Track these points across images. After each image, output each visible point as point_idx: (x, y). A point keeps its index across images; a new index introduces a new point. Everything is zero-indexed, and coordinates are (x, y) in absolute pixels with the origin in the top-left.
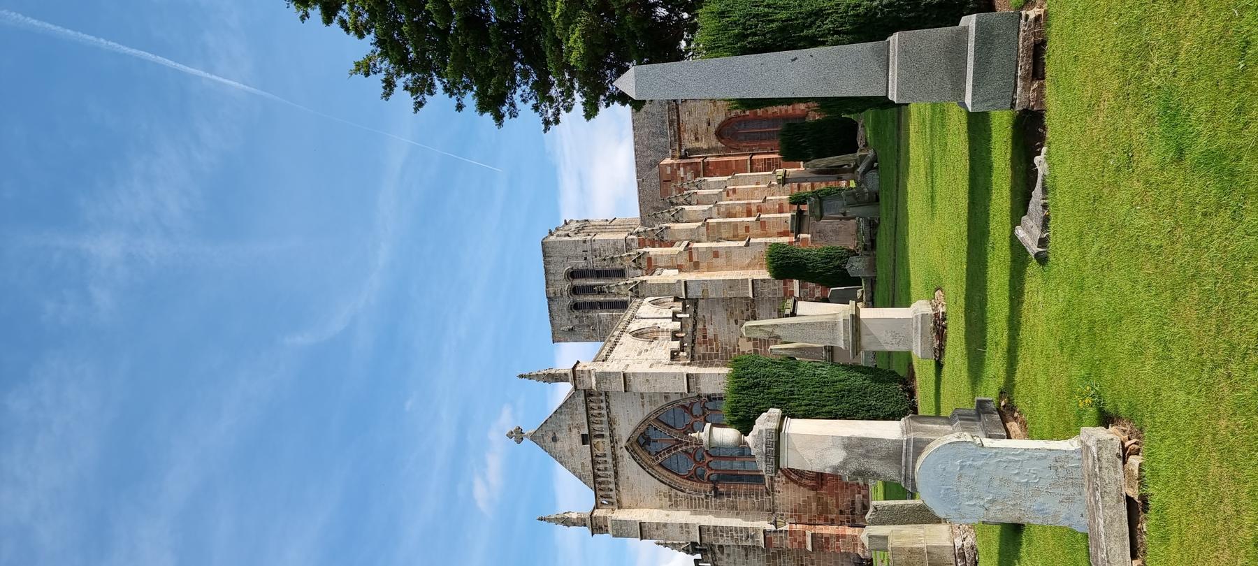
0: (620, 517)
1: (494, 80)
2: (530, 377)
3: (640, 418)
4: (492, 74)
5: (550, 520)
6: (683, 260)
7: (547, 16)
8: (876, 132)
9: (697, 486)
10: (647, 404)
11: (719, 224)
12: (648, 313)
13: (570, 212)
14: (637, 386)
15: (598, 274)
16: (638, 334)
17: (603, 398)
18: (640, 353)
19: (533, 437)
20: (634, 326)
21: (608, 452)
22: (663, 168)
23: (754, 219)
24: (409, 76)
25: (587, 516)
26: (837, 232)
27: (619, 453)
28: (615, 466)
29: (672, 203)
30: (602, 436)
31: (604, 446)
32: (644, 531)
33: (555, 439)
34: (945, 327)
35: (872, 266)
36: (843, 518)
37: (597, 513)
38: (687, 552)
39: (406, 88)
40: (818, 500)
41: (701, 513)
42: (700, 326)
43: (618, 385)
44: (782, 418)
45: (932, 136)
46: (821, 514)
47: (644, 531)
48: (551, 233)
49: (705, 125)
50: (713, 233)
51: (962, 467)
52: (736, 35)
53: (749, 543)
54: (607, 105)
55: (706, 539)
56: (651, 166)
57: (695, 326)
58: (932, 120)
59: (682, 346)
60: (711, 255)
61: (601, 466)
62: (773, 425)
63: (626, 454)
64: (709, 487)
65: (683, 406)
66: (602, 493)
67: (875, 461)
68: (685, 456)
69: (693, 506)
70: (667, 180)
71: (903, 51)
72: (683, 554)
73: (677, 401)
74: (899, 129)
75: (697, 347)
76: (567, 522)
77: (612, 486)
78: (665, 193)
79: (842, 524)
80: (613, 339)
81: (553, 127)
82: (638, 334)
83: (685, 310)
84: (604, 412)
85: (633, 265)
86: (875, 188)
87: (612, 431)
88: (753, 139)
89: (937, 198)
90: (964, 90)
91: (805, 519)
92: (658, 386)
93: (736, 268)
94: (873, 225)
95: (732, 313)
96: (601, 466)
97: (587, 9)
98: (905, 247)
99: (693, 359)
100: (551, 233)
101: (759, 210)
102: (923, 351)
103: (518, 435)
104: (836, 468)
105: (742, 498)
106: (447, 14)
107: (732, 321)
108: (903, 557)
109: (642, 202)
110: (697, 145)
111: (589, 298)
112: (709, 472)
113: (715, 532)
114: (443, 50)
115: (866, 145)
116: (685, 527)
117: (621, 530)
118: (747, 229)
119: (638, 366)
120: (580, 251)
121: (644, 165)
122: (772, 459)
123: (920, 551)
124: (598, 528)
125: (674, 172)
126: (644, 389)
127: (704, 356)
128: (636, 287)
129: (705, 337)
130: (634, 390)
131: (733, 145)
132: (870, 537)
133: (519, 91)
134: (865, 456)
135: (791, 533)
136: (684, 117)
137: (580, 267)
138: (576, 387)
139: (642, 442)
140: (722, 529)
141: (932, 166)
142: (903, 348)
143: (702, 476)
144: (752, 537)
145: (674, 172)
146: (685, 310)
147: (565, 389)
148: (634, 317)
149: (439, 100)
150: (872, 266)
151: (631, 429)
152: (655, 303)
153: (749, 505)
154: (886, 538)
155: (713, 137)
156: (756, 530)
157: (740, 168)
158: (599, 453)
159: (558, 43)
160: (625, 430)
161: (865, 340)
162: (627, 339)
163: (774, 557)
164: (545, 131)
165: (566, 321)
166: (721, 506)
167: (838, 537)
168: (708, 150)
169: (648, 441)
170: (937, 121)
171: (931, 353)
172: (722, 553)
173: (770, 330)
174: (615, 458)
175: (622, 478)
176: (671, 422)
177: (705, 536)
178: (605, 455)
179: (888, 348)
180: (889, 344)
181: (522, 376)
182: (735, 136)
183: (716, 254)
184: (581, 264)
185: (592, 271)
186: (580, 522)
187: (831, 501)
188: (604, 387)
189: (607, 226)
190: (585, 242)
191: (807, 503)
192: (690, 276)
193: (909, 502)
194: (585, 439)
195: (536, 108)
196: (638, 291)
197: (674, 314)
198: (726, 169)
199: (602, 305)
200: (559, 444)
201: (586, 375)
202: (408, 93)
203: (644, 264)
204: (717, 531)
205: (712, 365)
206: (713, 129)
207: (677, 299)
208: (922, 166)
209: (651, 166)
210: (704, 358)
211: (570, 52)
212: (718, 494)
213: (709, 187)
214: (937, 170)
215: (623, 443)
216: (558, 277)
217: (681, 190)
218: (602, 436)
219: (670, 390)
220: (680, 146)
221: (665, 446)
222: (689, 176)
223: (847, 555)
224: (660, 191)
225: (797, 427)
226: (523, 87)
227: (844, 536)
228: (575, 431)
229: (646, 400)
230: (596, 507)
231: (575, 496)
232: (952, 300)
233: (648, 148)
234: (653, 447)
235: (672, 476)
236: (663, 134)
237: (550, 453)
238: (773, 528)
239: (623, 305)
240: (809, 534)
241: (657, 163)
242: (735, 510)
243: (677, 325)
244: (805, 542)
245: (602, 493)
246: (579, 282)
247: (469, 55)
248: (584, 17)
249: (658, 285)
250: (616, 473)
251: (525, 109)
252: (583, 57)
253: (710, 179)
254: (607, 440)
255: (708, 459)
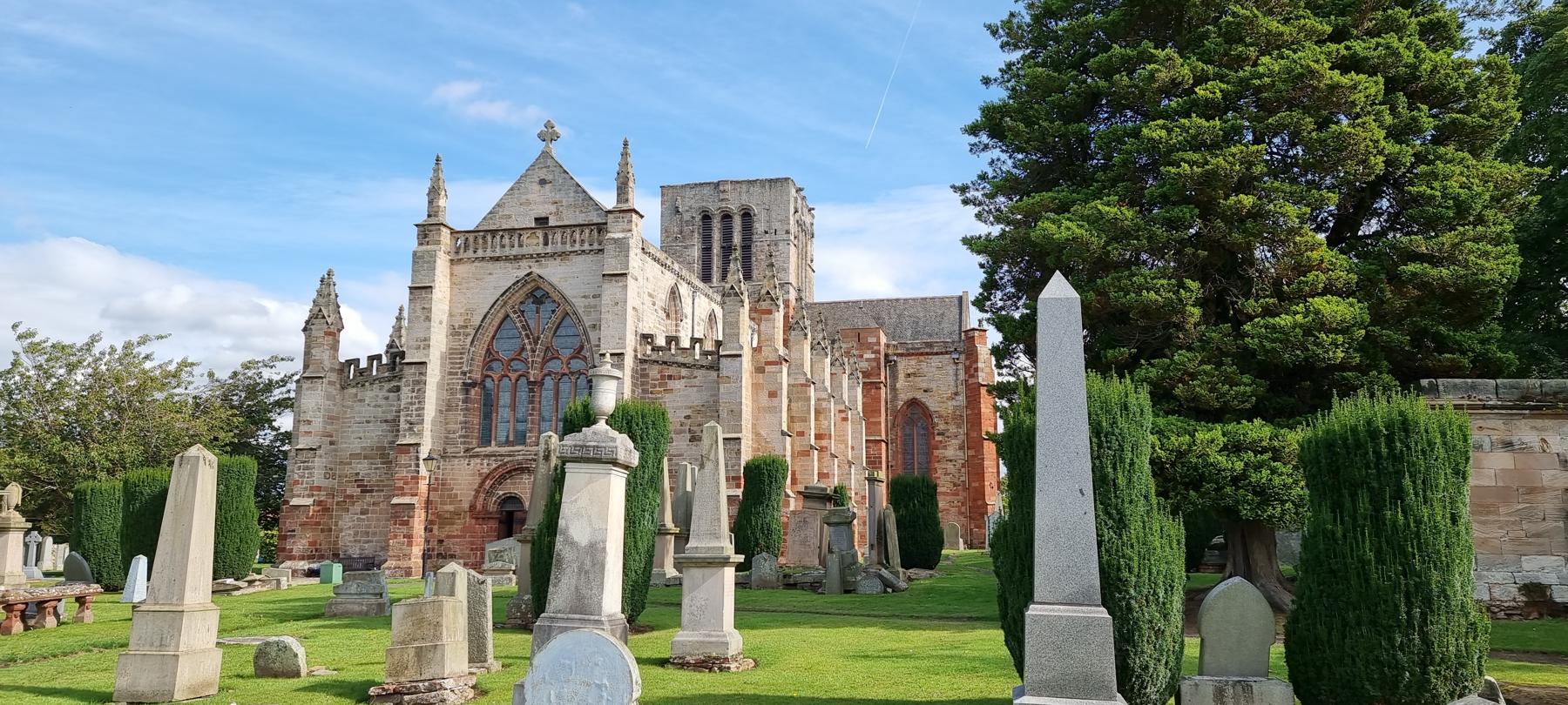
0: (439, 262)
1: (1021, 126)
2: (625, 155)
3: (568, 293)
4: (1029, 123)
5: (436, 171)
6: (767, 354)
7: (1098, 195)
8: (929, 591)
9: (479, 361)
10: (587, 302)
11: (809, 399)
12: (701, 311)
13: (825, 218)
14: (610, 290)
15: (747, 248)
16: (674, 294)
17: (596, 246)
18: (650, 295)
19: (546, 154)
20: (684, 289)
21: (525, 250)
22: (875, 332)
23: (813, 442)
24: (1028, 19)
25: (441, 220)
26: (804, 542)
27: (524, 263)
28: (507, 259)
29: (833, 342)
30: (546, 244)
31: (533, 244)
32: (420, 291)
33: (543, 182)
34: (711, 670)
35: (764, 585)
36: (434, 543)
37: (445, 232)
38: (390, 346)
39: (1012, 15)
40: (457, 514)
41: (442, 365)
42: (684, 372)
43: (611, 265)
44: (627, 467)
45: (942, 658)
46: (439, 516)
47: (420, 291)
48: (799, 190)
49: (924, 385)
50: (799, 391)
51: (599, 686)
52: (1099, 423)
53: (403, 425)
54: (982, 266)
55: (409, 371)
56: (877, 319)
57: (684, 365)
58: (961, 658)
59: (659, 349)
60: (773, 389)
61: (506, 240)
62: (621, 457)
63: (522, 273)
64: (477, 376)
65: (582, 347)
66: (471, 239)
67: (574, 582)
68: (517, 347)
69: (453, 355)
70: (860, 337)
71: (1089, 623)
72: (387, 341)
73: (588, 341)
74: (940, 618)
75: (657, 367)
76: (434, 193)
77: (480, 253)
78: (845, 334)
79: (427, 541)
80: (669, 263)
81: (958, 197)
82: (674, 294)
83: (705, 354)
84: (577, 247)
85: (763, 291)
86: (861, 589)
87: (553, 255)
88: (904, 444)
89: (868, 663)
90: (1039, 695)
91: (434, 497)
92: (610, 317)
93: (755, 418)
94: (815, 586)
95: (699, 412)
96: (506, 240)
97: (1107, 243)
98: (798, 624)
99: (643, 361)
100: (799, 190)
101: (822, 450)
102: (683, 644)
103: (548, 135)
104: (565, 533)
105: (461, 418)
106: (1107, 72)
107: (689, 412)
108: (429, 615)
109: (834, 305)
110: (901, 376)
111: (717, 236)
112: (496, 377)
113: (418, 382)
114: (1056, 65)
115: (910, 579)
116: (425, 343)
117: (422, 262)
118: (801, 434)
119: (635, 292)
120: (776, 225)
121: (875, 308)
122: (578, 454)
123: (438, 636)
124: (426, 231)
125: (869, 346)
126: (606, 299)
127: (647, 376)
128: (736, 294)
129: (670, 377)
130: (605, 286)
131: (899, 419)
132: (453, 574)
133: (1004, 156)
134: (580, 569)
135: (416, 478)
136: (935, 361)
137: (756, 225)
138: (610, 212)
139: (537, 294)
140: (421, 392)
141: (905, 657)
142: (685, 618)
143: (490, 369)
144: (410, 429)
145: (869, 346)
146: (705, 354)
147: (608, 200)
148: (695, 289)
149: (996, 58)
150: (764, 585)
151: (554, 280)
152: (712, 317)
153: (452, 426)
154: (452, 593)
155: (910, 396)
156: (420, 434)
157: (872, 427)
158: (524, 238)
159: (1063, 208)
160: (553, 273)
161: (696, 573)
162: (668, 279)
163: (383, 456)
164: (953, 187)
165: (690, 205)
166: (451, 391)
167: (409, 537)
168: (894, 389)
169: (539, 301)
170: (962, 664)
171: (678, 652)
172: (390, 391)
173: (712, 457)
174: (516, 258)
175: (490, 265)
176: (561, 332)
177: (413, 370)
178: (521, 246)
179: (686, 601)
180: (690, 602)
181: (626, 144)
182: (910, 422)
183: (773, 395)
184: (759, 227)
185: (750, 240)
186: (433, 210)
187: (456, 529)
188: (609, 248)
189: (806, 261)
190: (788, 232)
191: (453, 499)
192: (747, 362)
193: (490, 624)
194: (542, 221)
195: (983, 177)
196: (729, 296)
197: (700, 340)
198: (870, 410)
199: (707, 250)
200: (536, 187)
201: (626, 227)
202: (1005, 17)
203: (764, 305)
204: (420, 384)
205: (634, 385)
206: (919, 395)
207: (719, 344)
208: (901, 645)
209: (877, 319)
210: (643, 376)
211: (1054, 222)
212: (467, 387)
213: (851, 388)
214: (902, 663)
215: (536, 270)
216: (744, 197)
217: (848, 353)
218: (546, 244)
219: (604, 332)
220: (901, 355)
221: (532, 324)
222: (864, 365)
223: (385, 548)
224: (846, 328)
225: (617, 483)
226: (1010, 162)
227: (410, 544)
228: (553, 208)
229: (592, 301)
230: (453, 232)
231: (468, 205)
232: (748, 678)
233: (899, 316)
234: (530, 307)
235: (492, 330)
236: (916, 334)
237: (524, 176)
238: (424, 455)
239: (706, 277)
240: (414, 500)
241: (881, 325)
242: (447, 408)
243: (686, 343)
244: (403, 495)
245: (471, 239)
246: (737, 223)
247: (1055, 97)
248: (1096, 241)
249: (737, 322)
250: (498, 259)
251: (982, 163)
252: (1048, 238)
253: (859, 390)
254: (540, 249)
255: (513, 376)
